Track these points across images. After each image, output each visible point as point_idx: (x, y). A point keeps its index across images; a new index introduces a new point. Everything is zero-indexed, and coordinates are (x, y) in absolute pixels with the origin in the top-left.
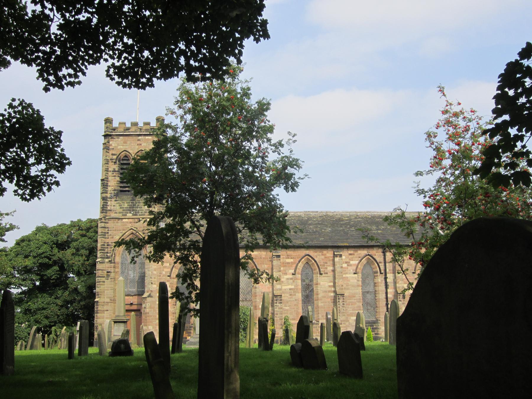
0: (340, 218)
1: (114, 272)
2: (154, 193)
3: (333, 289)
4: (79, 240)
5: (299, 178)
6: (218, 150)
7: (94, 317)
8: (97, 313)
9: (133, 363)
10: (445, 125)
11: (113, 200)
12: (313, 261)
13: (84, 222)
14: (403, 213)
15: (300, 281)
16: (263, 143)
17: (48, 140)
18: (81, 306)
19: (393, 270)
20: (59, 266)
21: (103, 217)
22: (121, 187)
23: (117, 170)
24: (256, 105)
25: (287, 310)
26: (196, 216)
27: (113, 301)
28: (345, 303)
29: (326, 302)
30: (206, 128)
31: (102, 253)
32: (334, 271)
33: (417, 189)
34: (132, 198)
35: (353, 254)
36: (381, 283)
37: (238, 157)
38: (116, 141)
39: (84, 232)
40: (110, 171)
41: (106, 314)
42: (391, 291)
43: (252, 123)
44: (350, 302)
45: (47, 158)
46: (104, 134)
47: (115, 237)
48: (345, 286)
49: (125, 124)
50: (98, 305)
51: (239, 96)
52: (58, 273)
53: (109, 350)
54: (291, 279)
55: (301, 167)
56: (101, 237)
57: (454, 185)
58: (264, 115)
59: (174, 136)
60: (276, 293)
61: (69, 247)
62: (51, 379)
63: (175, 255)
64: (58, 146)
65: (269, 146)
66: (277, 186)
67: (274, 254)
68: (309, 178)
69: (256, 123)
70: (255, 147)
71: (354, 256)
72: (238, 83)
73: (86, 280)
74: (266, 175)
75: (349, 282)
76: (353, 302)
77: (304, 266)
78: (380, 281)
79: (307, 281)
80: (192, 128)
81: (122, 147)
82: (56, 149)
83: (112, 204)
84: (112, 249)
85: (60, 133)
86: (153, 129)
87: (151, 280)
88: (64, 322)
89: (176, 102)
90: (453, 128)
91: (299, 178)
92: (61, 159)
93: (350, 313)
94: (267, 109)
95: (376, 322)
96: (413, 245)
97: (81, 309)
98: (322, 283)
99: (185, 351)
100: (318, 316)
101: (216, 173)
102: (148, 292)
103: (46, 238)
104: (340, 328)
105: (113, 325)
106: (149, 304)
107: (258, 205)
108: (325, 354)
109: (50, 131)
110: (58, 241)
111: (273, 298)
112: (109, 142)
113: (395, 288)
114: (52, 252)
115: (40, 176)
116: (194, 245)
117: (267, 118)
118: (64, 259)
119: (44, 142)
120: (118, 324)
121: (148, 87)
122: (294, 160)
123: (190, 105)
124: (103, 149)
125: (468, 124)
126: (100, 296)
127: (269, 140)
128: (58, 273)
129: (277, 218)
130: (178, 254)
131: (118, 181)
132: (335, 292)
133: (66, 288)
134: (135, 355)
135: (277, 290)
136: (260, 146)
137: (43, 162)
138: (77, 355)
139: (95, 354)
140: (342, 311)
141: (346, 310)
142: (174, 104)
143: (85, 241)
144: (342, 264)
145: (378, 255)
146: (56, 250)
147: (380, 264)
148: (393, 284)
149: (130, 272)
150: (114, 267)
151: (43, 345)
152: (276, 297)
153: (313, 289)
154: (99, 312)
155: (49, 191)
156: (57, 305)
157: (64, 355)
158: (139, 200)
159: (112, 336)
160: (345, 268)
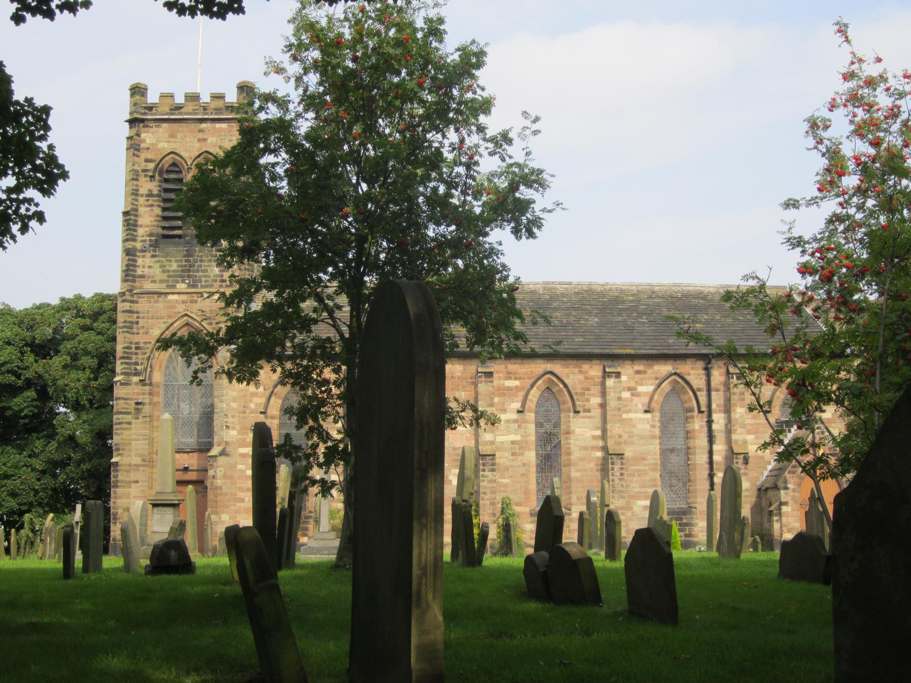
0: (618, 297)
1: (150, 404)
2: (238, 238)
3: (601, 443)
4: (78, 338)
5: (544, 210)
6: (374, 149)
7: (109, 495)
8: (117, 487)
9: (198, 589)
10: (848, 104)
11: (148, 254)
12: (561, 386)
13: (89, 299)
14: (763, 286)
15: (534, 426)
16: (469, 135)
17: (23, 125)
18: (83, 472)
19: (725, 406)
20: (37, 391)
21: (128, 290)
22: (164, 228)
23: (155, 192)
24: (456, 56)
25: (506, 485)
26: (327, 287)
27: (149, 462)
28: (626, 473)
29: (585, 470)
30: (351, 103)
31: (126, 363)
32: (603, 406)
33: (787, 235)
34: (187, 251)
35: (645, 372)
36: (701, 432)
37: (416, 164)
38: (153, 133)
39: (88, 321)
40: (142, 195)
41: (134, 490)
42: (719, 448)
43: (446, 94)
44: (635, 470)
45: (20, 163)
46: (128, 117)
47: (152, 331)
48: (625, 436)
49: (172, 96)
50: (117, 471)
51: (420, 35)
52: (34, 403)
53: (145, 562)
54: (515, 421)
55: (548, 186)
56: (123, 332)
57: (863, 230)
58: (473, 77)
59: (281, 119)
60: (484, 449)
61: (57, 352)
62: (35, 619)
63: (283, 369)
64: (43, 138)
65: (481, 142)
66: (496, 227)
67: (480, 370)
68: (563, 209)
69: (455, 92)
70: (451, 144)
71: (646, 376)
72: (419, 9)
73: (92, 420)
74: (475, 203)
75: (633, 430)
76: (642, 470)
77: (541, 395)
78: (697, 427)
79: (548, 427)
80: (320, 103)
81: (166, 145)
82: (38, 144)
83: (146, 264)
84: (146, 356)
85: (46, 110)
86: (230, 108)
87: (226, 420)
88: (47, 504)
89: (286, 46)
90: (864, 110)
91: (544, 210)
92: (48, 165)
93: (636, 492)
94: (478, 66)
95: (688, 511)
96: (774, 353)
97: (82, 478)
98: (578, 431)
99: (303, 566)
100: (570, 498)
101: (368, 197)
102: (219, 445)
103: (9, 334)
104: (620, 522)
105: (150, 512)
106: (222, 469)
107: (456, 267)
108: (598, 573)
109: (25, 106)
110: (34, 338)
111: (477, 460)
112: (138, 135)
113: (729, 442)
114: (22, 361)
115: (4, 201)
116: (323, 351)
117: (480, 82)
118: (47, 375)
119: (14, 129)
120: (160, 508)
121: (230, 13)
122: (533, 172)
123: (316, 54)
124: (127, 149)
125: (898, 103)
126: (121, 452)
127: (481, 129)
128: (34, 403)
129: (495, 292)
130: (289, 365)
131: (158, 216)
132: (605, 449)
133: (51, 436)
134: (198, 572)
135: (486, 443)
136: (462, 141)
137: (10, 172)
138: (81, 570)
139: (116, 570)
140: (618, 488)
141: (627, 486)
142: (283, 52)
143: (91, 340)
144: (620, 392)
145: (695, 374)
146: (30, 358)
147: (698, 393)
148: (723, 435)
149: (182, 405)
150: (150, 394)
151: (7, 551)
152: (485, 459)
153: (560, 441)
154: (119, 484)
155: (23, 233)
156: (33, 470)
157: (53, 571)
158: (201, 256)
159: (149, 533)
160: (626, 400)
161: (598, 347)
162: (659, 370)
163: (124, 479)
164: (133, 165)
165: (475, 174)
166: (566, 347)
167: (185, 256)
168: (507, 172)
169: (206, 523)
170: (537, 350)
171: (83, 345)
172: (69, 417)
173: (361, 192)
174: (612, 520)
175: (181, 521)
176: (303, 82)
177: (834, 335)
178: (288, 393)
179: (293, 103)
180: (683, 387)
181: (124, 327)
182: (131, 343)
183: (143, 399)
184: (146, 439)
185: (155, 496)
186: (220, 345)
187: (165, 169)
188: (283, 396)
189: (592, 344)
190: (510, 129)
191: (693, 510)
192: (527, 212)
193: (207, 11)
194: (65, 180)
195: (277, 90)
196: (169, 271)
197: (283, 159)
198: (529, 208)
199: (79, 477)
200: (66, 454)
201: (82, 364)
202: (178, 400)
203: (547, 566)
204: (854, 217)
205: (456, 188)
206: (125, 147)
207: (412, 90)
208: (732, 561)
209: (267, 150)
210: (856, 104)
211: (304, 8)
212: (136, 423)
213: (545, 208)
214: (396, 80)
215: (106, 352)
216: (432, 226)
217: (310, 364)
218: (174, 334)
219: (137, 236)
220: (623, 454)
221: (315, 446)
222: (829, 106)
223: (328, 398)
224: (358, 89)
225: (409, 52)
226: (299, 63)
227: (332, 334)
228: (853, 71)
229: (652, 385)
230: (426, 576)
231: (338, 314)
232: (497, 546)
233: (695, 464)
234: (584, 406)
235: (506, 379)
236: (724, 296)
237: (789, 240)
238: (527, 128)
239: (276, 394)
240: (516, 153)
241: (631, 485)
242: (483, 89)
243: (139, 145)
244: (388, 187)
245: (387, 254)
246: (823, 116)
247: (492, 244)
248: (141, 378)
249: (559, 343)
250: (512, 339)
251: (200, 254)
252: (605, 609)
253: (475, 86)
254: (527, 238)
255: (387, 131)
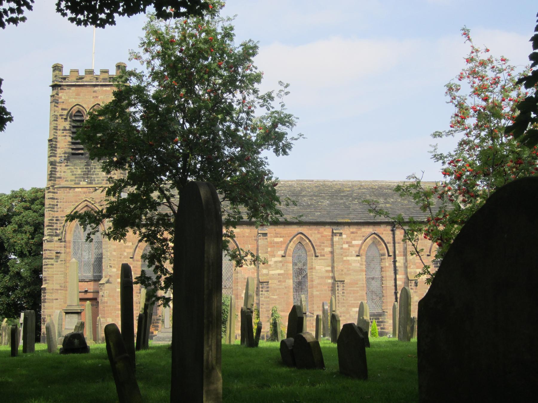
3: (331, 275)
4: (22, 214)
6: (193, 103)
7: (40, 307)
8: (45, 302)
9: (90, 362)
10: (470, 76)
11: (63, 165)
12: (308, 241)
13: (28, 191)
14: (419, 182)
15: (291, 265)
16: (248, 95)
18: (25, 294)
19: (404, 252)
22: (73, 149)
23: (68, 128)
24: (240, 49)
25: (275, 299)
30: (179, 77)
31: (50, 229)
32: (332, 253)
33: (434, 154)
34: (86, 162)
35: (356, 233)
37: (218, 112)
39: (28, 204)
40: (60, 130)
43: (235, 71)
46: (51, 84)
48: (345, 270)
49: (77, 71)
50: (45, 293)
51: (219, 37)
53: (60, 346)
54: (281, 262)
55: (295, 125)
56: (48, 211)
57: (479, 149)
58: (250, 61)
59: (138, 86)
60: (262, 279)
61: (10, 223)
63: (140, 232)
65: (256, 99)
67: (259, 232)
68: (304, 138)
69: (240, 70)
71: (357, 235)
72: (219, 21)
73: (30, 263)
74: (252, 134)
75: (350, 267)
79: (300, 265)
80: (161, 76)
81: (74, 100)
83: (62, 170)
84: (62, 225)
87: (110, 262)
89: (141, 44)
90: (479, 80)
94: (254, 55)
97: (25, 297)
99: (152, 348)
100: (313, 307)
101: (190, 131)
102: (106, 277)
104: (339, 321)
105: (64, 317)
106: (108, 292)
107: (241, 172)
112: (57, 94)
113: (406, 273)
116: (163, 220)
117: (254, 64)
120: (70, 315)
121: (107, 24)
123: (158, 48)
124: (51, 103)
125: (498, 75)
127: (255, 92)
130: (143, 230)
131: (69, 142)
132: (333, 278)
134: (91, 352)
136: (244, 99)
138: (22, 352)
140: (341, 301)
141: (347, 300)
142: (140, 47)
143: (30, 216)
144: (342, 245)
145: (385, 234)
147: (388, 245)
148: (403, 269)
149: (84, 253)
150: (65, 247)
153: (307, 274)
154: (46, 301)
157: (5, 352)
158: (95, 166)
159: (63, 329)
160: (345, 249)
161: (329, 218)
162: (365, 232)
163: (49, 298)
164: (54, 112)
165: (252, 118)
166: (310, 218)
167: (85, 166)
168: (271, 117)
169: (98, 323)
170: (288, 220)
171: (25, 218)
172: (17, 261)
173: (186, 129)
174: (334, 319)
175: (82, 322)
176: (151, 65)
177: (460, 210)
178: (147, 246)
179: (146, 76)
180: (379, 241)
181: (49, 208)
182: (53, 217)
183: (61, 250)
184: (62, 274)
185: (67, 307)
186: (104, 218)
187: (73, 114)
188: (143, 248)
189: (325, 216)
190: (272, 92)
191: (386, 313)
192: (283, 140)
193: (94, 23)
194: (11, 122)
195: (136, 69)
196: (76, 175)
197: (139, 110)
198: (284, 137)
199: (23, 297)
200: (15, 282)
201: (25, 230)
202: (82, 250)
203: (293, 346)
204: (474, 142)
205: (241, 126)
206: (50, 101)
207: (214, 69)
208: (405, 343)
209: (130, 105)
210: (475, 76)
211: (152, 21)
212: (56, 265)
213: (293, 137)
214: (206, 63)
215: (39, 223)
216: (226, 148)
217: (156, 229)
218: (76, 212)
219: (56, 154)
220: (344, 281)
221: (159, 278)
222: (459, 77)
223: (166, 249)
224: (183, 69)
225: (213, 46)
226: (149, 53)
227: (169, 211)
228: (472, 57)
229: (361, 240)
230: (212, 351)
231: (172, 200)
232: (269, 335)
233: (386, 286)
234: (321, 253)
235: (275, 237)
236: (396, 188)
237: (435, 155)
238: (282, 91)
239: (139, 247)
240: (276, 105)
241: (349, 299)
242: (256, 68)
243: (58, 100)
244: (201, 125)
245: (201, 164)
246: (456, 83)
247: (261, 158)
248: (60, 238)
249: (300, 216)
250: (274, 214)
251: (94, 164)
252: (327, 370)
253: (251, 66)
254: (283, 155)
255: (201, 93)
